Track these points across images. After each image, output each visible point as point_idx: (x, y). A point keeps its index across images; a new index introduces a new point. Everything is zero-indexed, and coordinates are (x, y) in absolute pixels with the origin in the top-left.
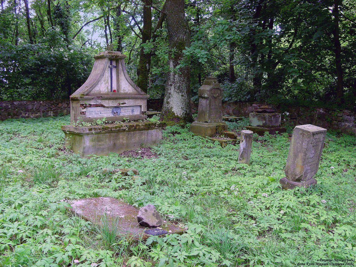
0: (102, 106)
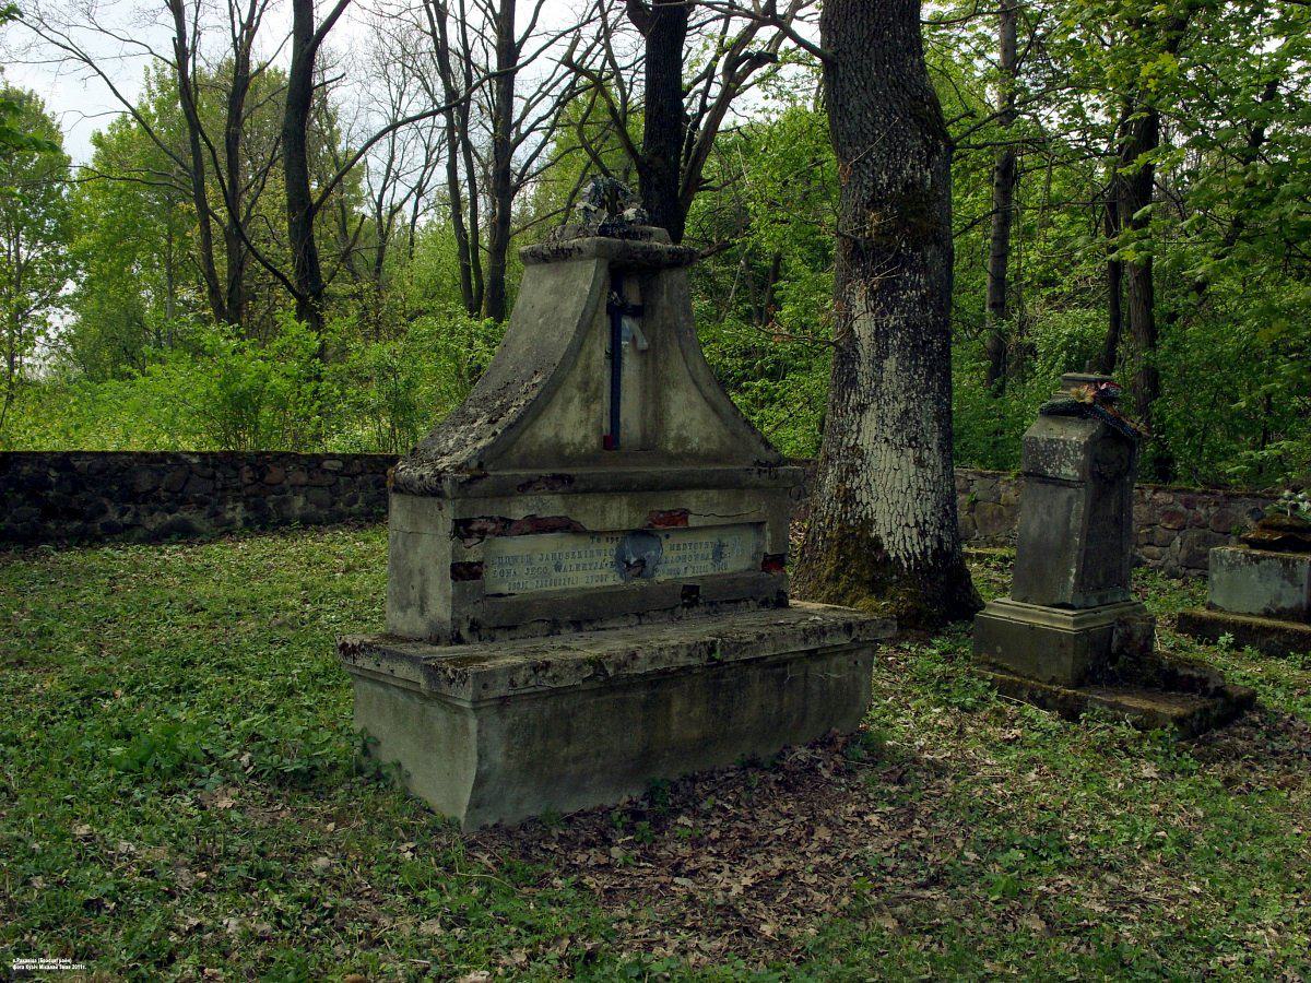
0: (567, 527)
